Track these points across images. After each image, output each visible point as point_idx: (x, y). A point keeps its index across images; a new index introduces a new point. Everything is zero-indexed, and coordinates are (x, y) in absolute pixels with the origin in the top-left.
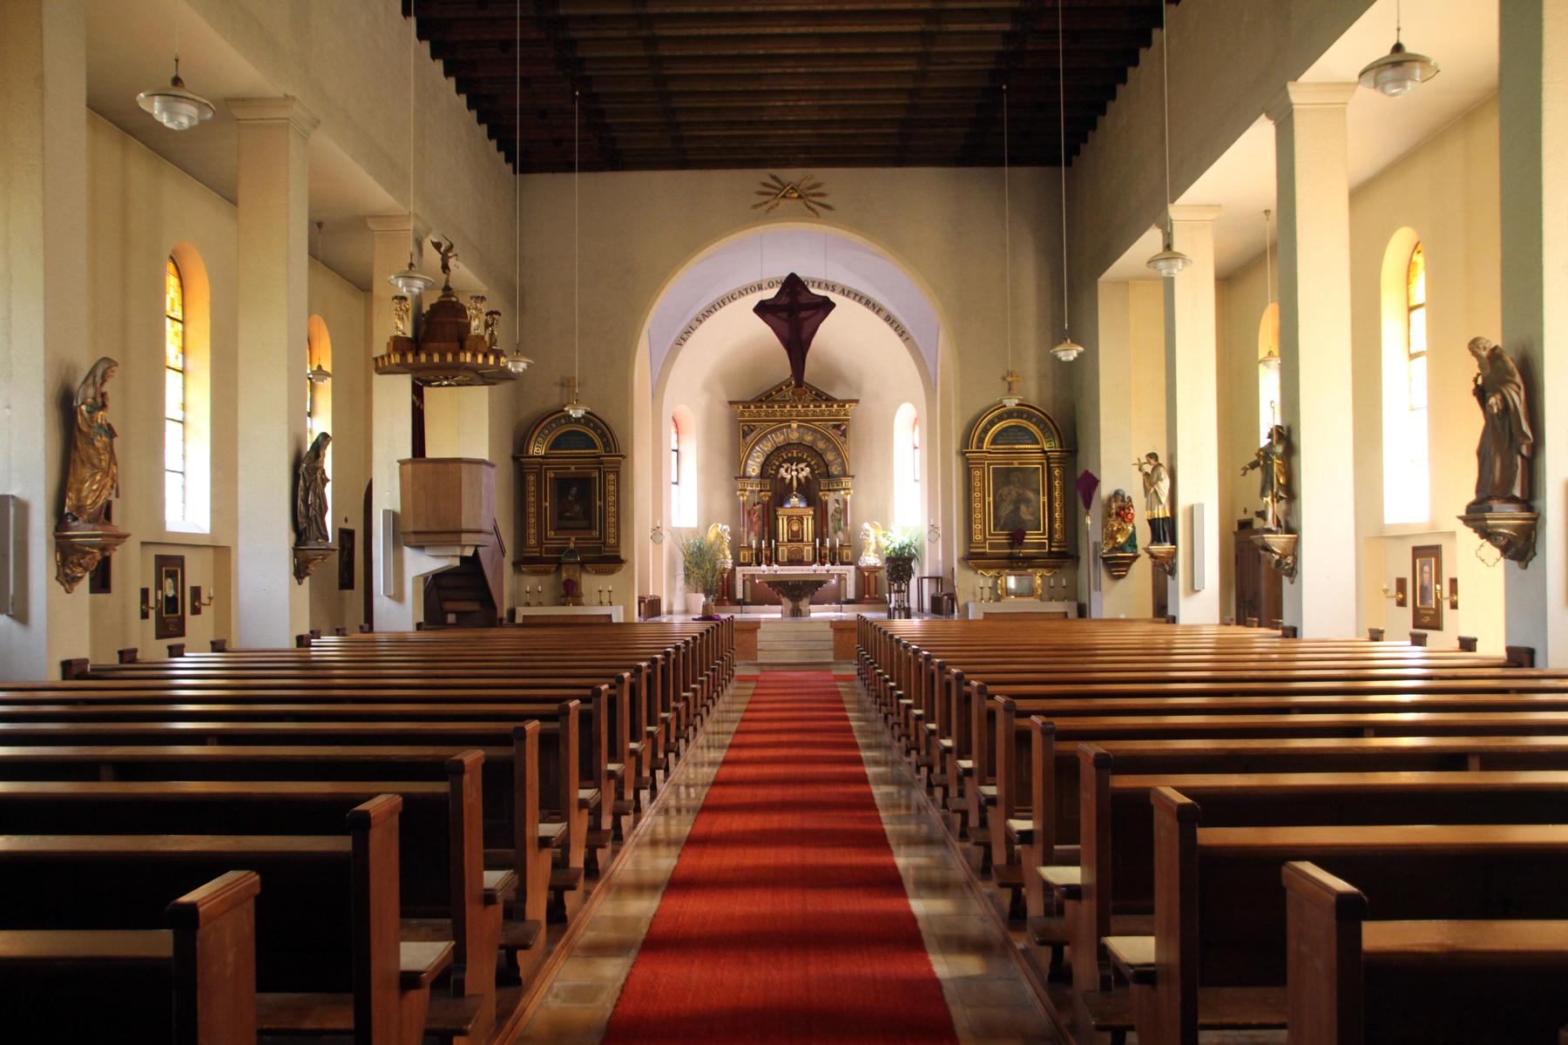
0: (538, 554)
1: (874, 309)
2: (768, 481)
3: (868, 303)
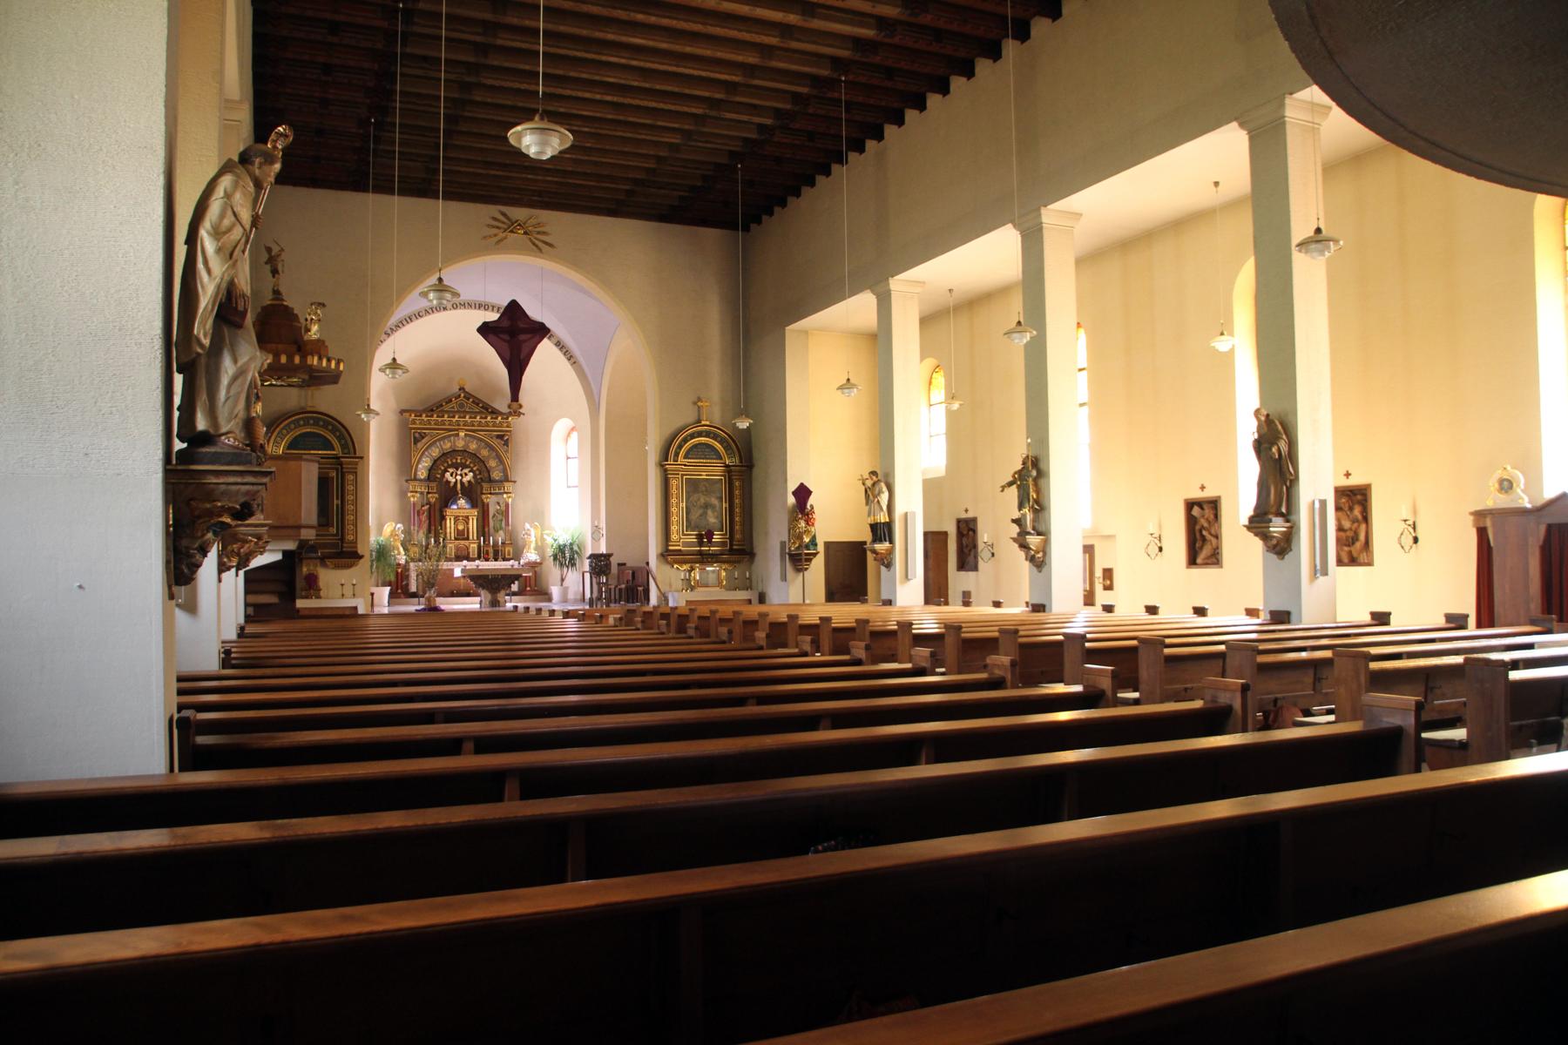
2: (434, 484)
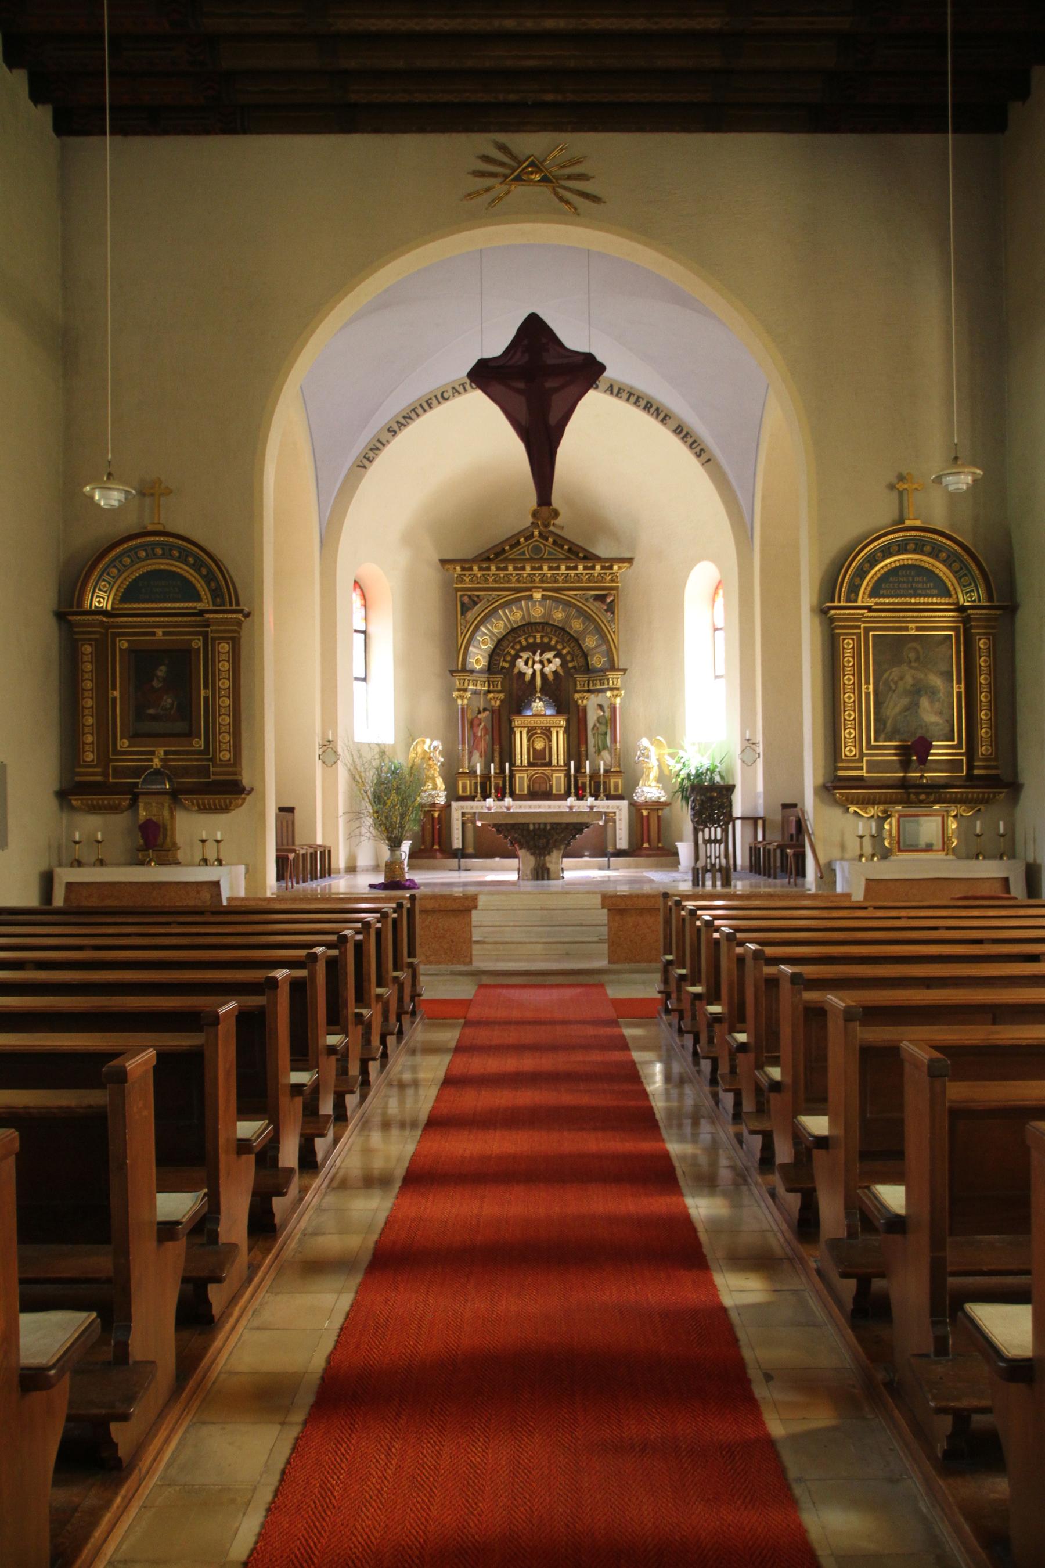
0: (99, 778)
1: (658, 415)
2: (498, 678)
3: (649, 406)
